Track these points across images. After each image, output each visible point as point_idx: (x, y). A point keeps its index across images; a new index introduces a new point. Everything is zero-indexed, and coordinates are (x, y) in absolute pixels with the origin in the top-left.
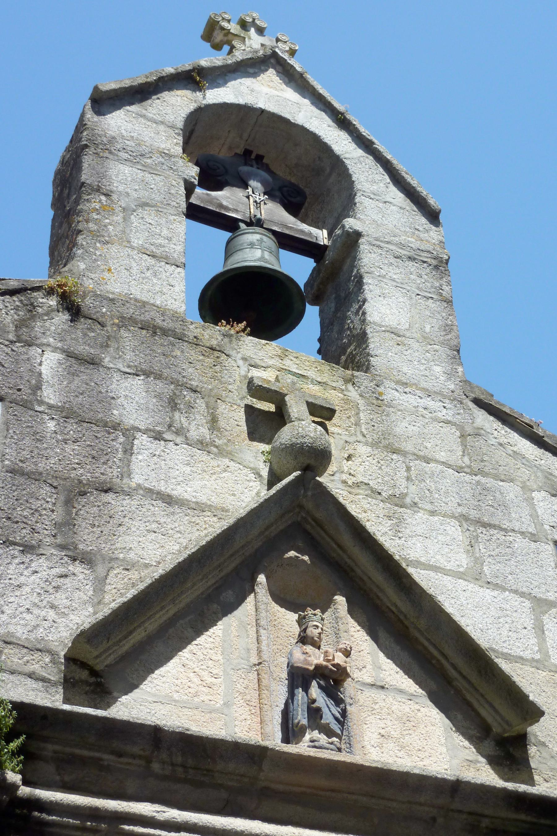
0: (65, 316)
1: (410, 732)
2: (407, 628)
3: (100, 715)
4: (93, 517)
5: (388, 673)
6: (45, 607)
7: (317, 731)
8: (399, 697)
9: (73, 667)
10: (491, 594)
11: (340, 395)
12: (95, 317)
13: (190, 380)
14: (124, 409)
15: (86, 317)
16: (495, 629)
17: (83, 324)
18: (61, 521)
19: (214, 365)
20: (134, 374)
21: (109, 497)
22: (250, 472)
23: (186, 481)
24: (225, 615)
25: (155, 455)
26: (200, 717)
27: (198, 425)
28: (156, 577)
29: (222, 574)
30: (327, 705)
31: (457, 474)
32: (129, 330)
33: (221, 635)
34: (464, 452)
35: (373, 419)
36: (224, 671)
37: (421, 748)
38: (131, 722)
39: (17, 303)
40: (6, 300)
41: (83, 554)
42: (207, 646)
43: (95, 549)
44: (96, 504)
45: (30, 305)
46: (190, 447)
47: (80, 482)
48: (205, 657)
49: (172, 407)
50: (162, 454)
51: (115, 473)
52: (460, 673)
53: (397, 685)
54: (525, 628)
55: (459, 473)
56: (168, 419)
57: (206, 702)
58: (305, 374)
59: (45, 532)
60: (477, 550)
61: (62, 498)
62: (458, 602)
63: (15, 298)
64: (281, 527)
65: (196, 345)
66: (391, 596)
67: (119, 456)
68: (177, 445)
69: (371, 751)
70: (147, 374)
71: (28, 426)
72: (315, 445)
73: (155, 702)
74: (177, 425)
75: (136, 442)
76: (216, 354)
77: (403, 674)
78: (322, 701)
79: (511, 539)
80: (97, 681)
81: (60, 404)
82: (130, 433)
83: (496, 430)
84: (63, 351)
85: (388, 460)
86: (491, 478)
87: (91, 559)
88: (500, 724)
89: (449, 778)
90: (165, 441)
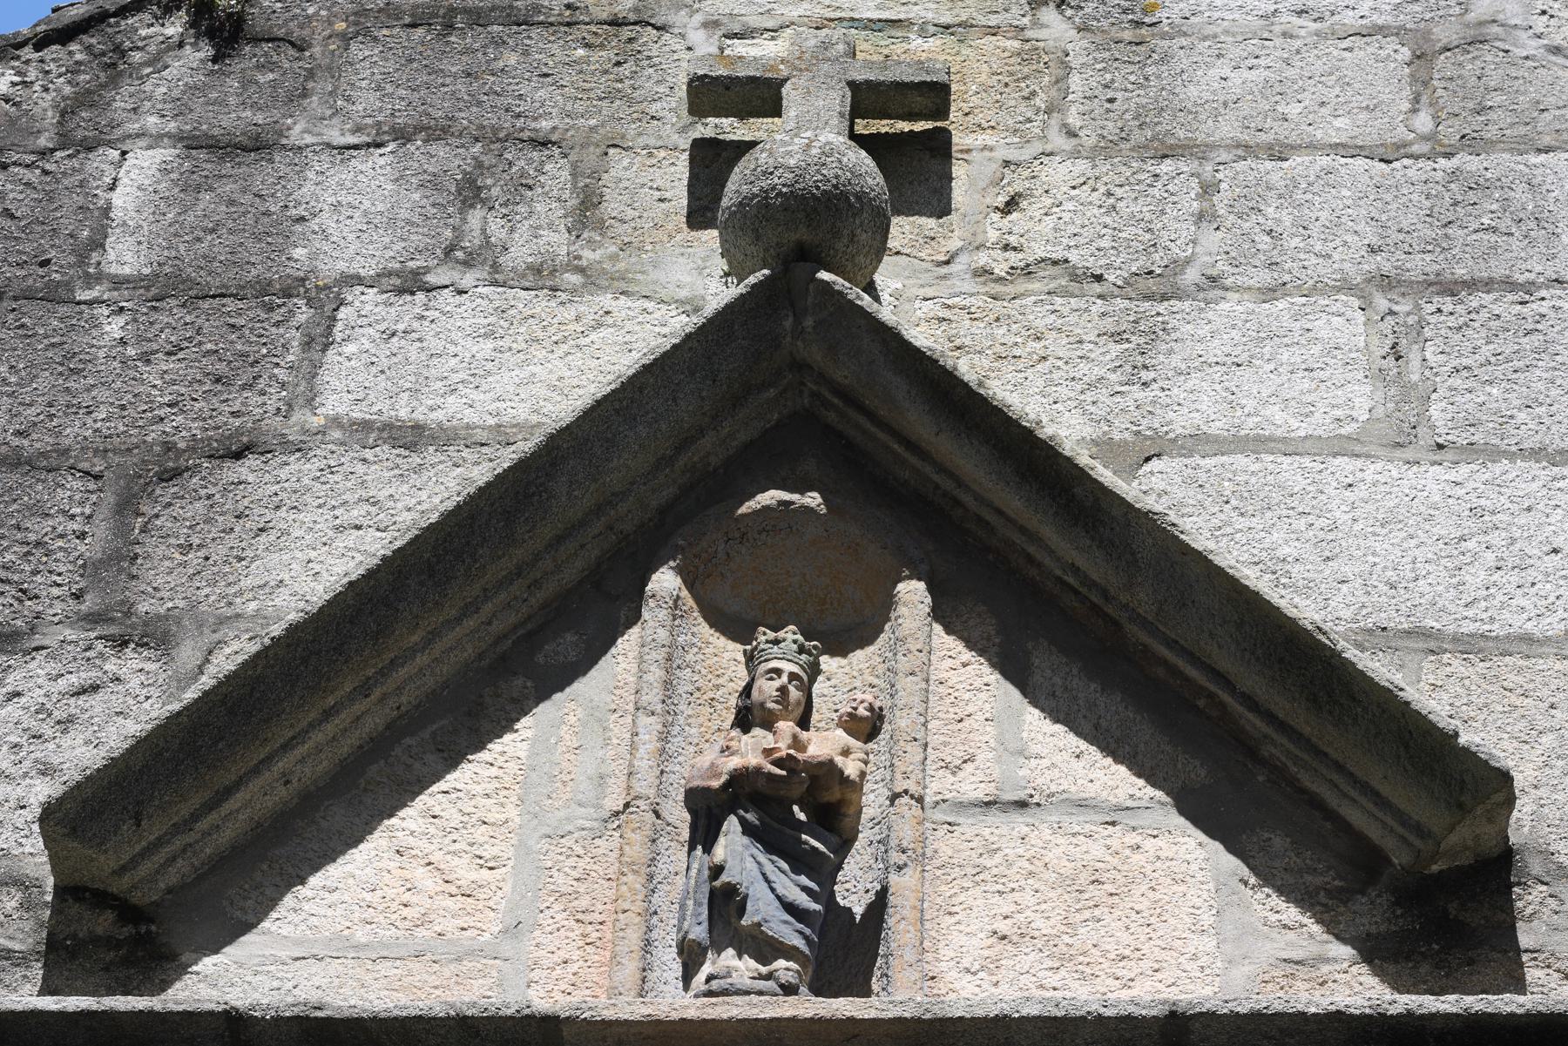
0: (197, 54)
1: (1097, 912)
2: (1116, 623)
3: (70, 1009)
4: (190, 527)
5: (1046, 762)
6: (25, 775)
7: (730, 951)
8: (1076, 822)
9: (74, 909)
10: (1447, 477)
11: (1009, 43)
12: (281, 33)
13: (535, 119)
14: (326, 238)
15: (257, 40)
16: (1444, 573)
17: (248, 57)
18: (99, 555)
19: (618, 64)
20: (368, 145)
21: (245, 470)
22: (674, 313)
23: (477, 376)
24: (543, 695)
25: (393, 335)
26: (425, 976)
27: (539, 227)
28: (275, 634)
29: (540, 596)
30: (764, 874)
31: (1383, 165)
32: (375, 39)
33: (522, 754)
34: (1416, 100)
35: (1113, 81)
36: (521, 846)
37: (1127, 952)
38: (159, 1013)
39: (78, 57)
40: (48, 58)
41: (146, 624)
42: (478, 789)
43: (181, 604)
44: (203, 492)
45: (113, 51)
46: (500, 289)
47: (168, 447)
48: (465, 819)
49: (464, 202)
50: (416, 325)
51: (272, 404)
52: (1270, 717)
53: (1073, 789)
54: (1555, 551)
55: (1388, 162)
56: (448, 233)
57: (449, 936)
58: (902, 16)
59: (55, 591)
60: (1415, 363)
61: (110, 498)
62: (1322, 522)
63: (74, 47)
64: (743, 437)
65: (569, 24)
66: (1062, 548)
67: (291, 358)
68: (461, 292)
69: (957, 986)
70: (403, 136)
71: (53, 345)
72: (801, 186)
73: (297, 959)
74: (472, 240)
75: (342, 314)
76: (626, 33)
77: (1099, 755)
78: (750, 864)
79: (1544, 308)
80: (138, 933)
81: (146, 271)
82: (327, 298)
83: (1544, 12)
84: (178, 138)
85: (1139, 182)
86: (1504, 150)
87: (166, 633)
88: (1403, 839)
89: (1144, 1012)
90: (428, 291)
